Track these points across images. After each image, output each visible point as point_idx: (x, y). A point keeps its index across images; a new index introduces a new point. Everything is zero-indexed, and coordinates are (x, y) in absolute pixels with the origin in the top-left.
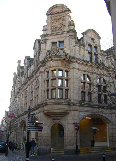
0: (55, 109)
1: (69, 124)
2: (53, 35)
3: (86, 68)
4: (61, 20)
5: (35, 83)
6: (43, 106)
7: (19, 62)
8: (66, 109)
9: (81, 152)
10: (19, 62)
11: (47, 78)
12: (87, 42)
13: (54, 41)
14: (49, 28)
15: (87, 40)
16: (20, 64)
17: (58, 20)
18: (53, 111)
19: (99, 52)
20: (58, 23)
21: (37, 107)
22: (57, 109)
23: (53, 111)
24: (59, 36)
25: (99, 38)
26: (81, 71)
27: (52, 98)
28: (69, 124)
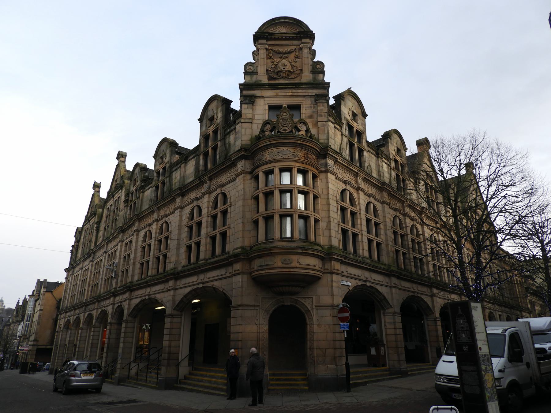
0: (293, 265)
1: (320, 307)
2: (273, 87)
3: (345, 176)
4: (292, 56)
5: (156, 228)
6: (250, 260)
7: (97, 186)
8: (317, 268)
9: (351, 382)
10: (97, 186)
11: (266, 188)
12: (346, 120)
13: (276, 101)
14: (262, 70)
15: (346, 110)
16: (99, 192)
17: (286, 55)
18: (287, 270)
19: (365, 145)
20: (284, 62)
21: (108, 294)
22: (298, 265)
23: (287, 270)
24: (289, 93)
25: (365, 115)
26: (338, 181)
27: (281, 238)
28: (320, 307)
